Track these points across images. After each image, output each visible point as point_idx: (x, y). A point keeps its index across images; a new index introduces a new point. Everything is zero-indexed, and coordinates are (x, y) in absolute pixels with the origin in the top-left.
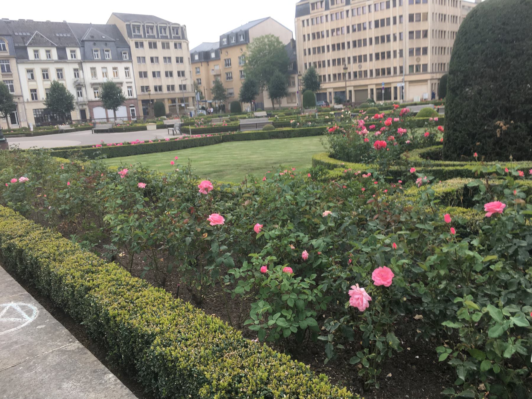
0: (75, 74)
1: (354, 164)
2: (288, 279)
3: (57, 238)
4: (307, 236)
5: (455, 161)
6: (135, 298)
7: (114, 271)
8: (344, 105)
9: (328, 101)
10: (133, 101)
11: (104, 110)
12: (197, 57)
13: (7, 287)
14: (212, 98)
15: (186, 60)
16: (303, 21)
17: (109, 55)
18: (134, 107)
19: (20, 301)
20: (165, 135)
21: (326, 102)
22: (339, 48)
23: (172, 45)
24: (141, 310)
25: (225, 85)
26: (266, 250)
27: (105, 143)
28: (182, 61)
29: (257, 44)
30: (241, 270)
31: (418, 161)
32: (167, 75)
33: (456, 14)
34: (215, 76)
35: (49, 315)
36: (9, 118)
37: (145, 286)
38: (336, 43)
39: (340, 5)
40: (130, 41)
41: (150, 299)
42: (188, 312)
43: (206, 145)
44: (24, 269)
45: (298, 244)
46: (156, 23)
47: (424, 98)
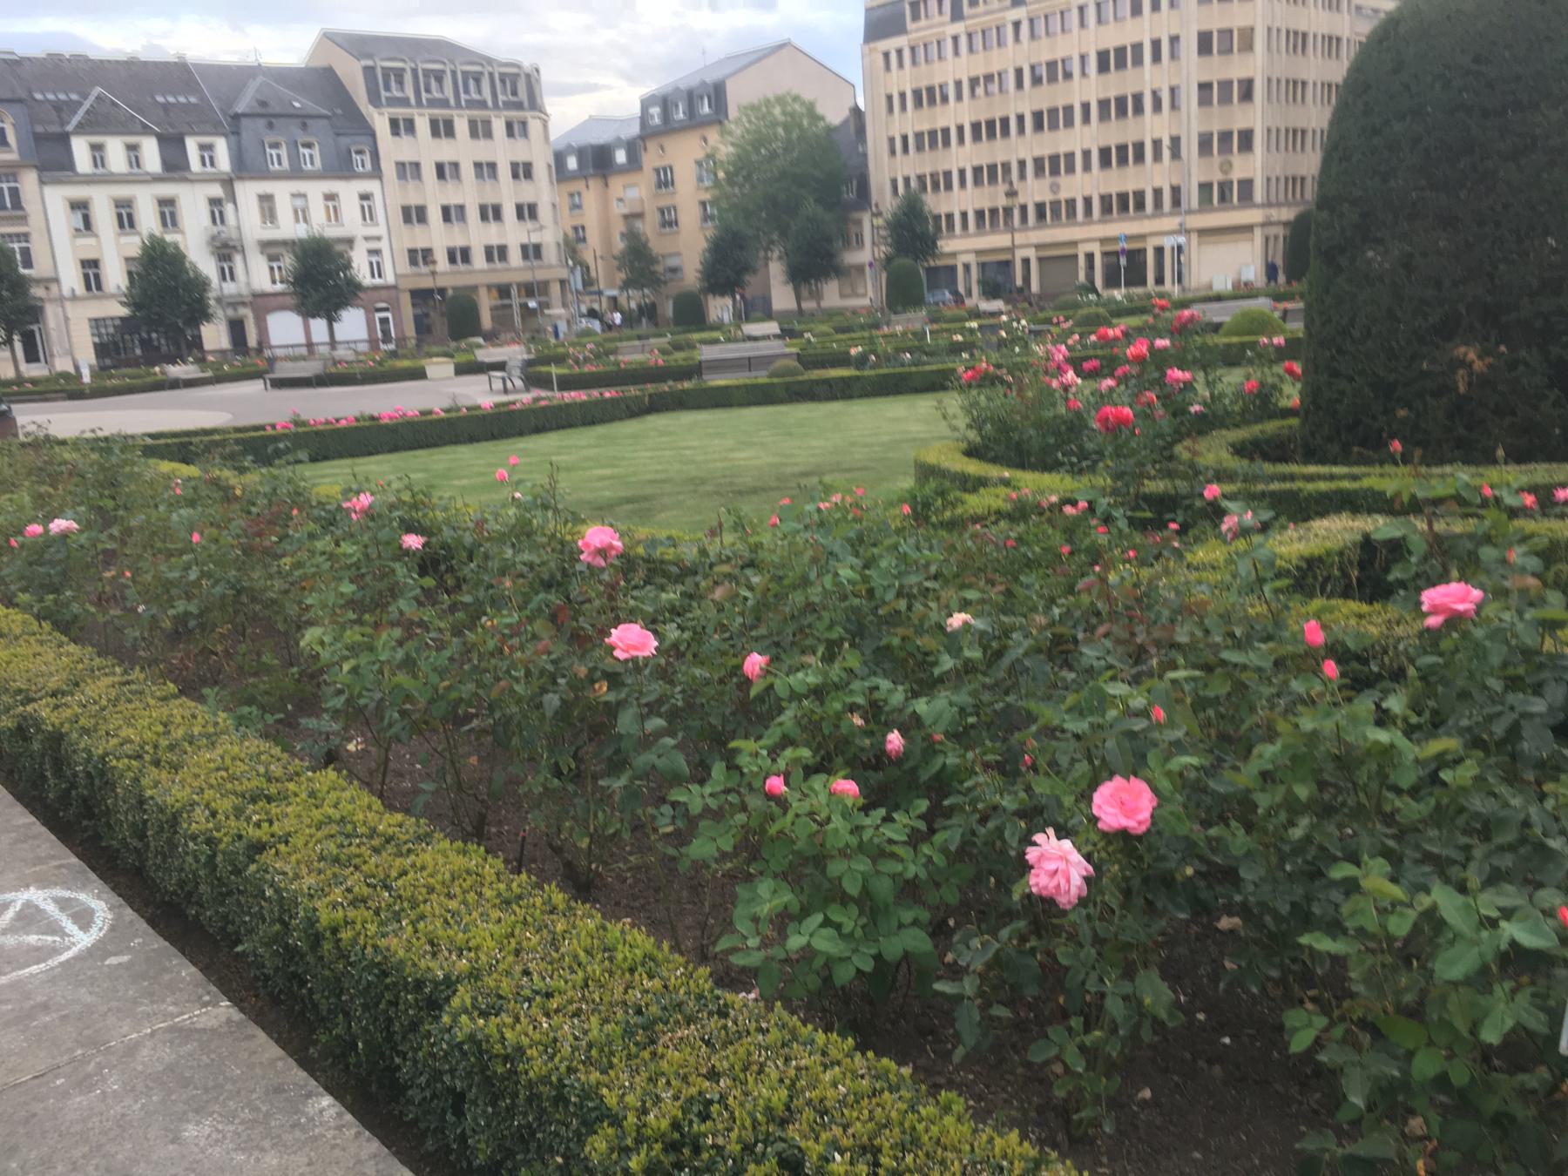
0: (213, 213)
2: (846, 815)
3: (164, 699)
4: (900, 688)
5: (1335, 463)
6: (394, 874)
7: (333, 795)
8: (1007, 302)
9: (961, 289)
10: (384, 293)
12: (572, 163)
14: (619, 283)
15: (541, 171)
16: (886, 55)
17: (313, 158)
18: (386, 310)
20: (480, 393)
21: (955, 293)
23: (498, 126)
25: (657, 245)
27: (304, 417)
29: (750, 122)
30: (708, 790)
32: (484, 217)
33: (1337, 32)
34: (626, 217)
36: (18, 346)
38: (983, 118)
40: (376, 116)
41: (439, 877)
42: (551, 912)
43: (602, 421)
45: (876, 713)
47: (1244, 278)
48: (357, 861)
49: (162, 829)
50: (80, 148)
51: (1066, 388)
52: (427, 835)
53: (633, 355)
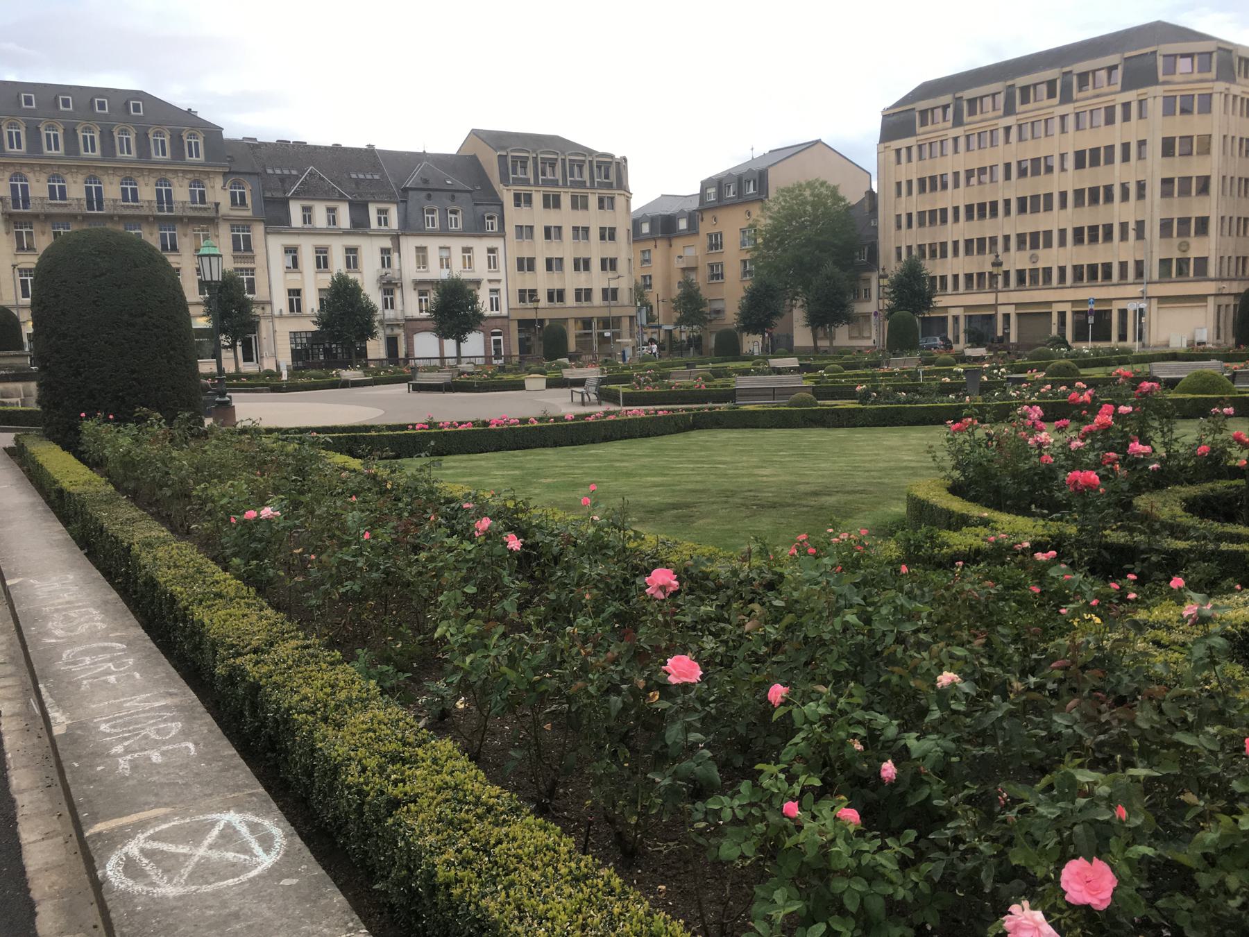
0: (383, 259)
2: (847, 838)
4: (895, 722)
6: (493, 842)
7: (450, 764)
8: (989, 350)
9: (950, 337)
10: (499, 322)
11: (437, 339)
12: (646, 228)
15: (622, 235)
16: (898, 151)
18: (499, 334)
20: (564, 405)
21: (945, 339)
22: (982, 215)
24: (506, 875)
25: (705, 292)
26: (794, 749)
27: (436, 420)
28: (612, 237)
29: (785, 201)
30: (736, 803)
31: (1179, 519)
32: (577, 268)
34: (684, 269)
35: (307, 853)
37: (515, 811)
38: (975, 201)
39: (991, 114)
41: (526, 850)
42: (610, 894)
43: (656, 434)
44: (258, 729)
45: (872, 738)
46: (563, 153)
47: (1197, 339)
50: (295, 210)
51: (1040, 446)
52: (518, 808)
53: (682, 379)
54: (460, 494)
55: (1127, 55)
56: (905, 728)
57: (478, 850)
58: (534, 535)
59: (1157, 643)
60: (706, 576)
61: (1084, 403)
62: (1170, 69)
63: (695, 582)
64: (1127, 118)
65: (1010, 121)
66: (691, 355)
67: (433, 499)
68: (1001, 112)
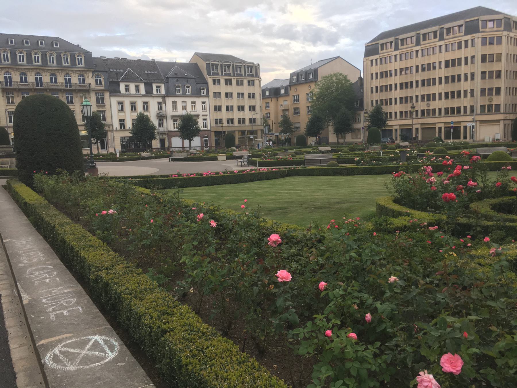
0: (158, 106)
1: (419, 212)
2: (352, 346)
3: (138, 274)
4: (371, 297)
6: (205, 347)
8: (410, 143)
9: (394, 138)
10: (207, 132)
12: (267, 93)
13: (93, 318)
14: (279, 131)
16: (372, 61)
18: (207, 137)
19: (104, 334)
20: (234, 166)
21: (391, 138)
22: (407, 87)
23: (245, 82)
24: (211, 361)
25: (292, 120)
26: (329, 308)
27: (181, 173)
29: (325, 82)
30: (306, 331)
31: (488, 213)
32: (239, 110)
34: (283, 110)
36: (99, 144)
37: (214, 334)
38: (404, 81)
42: (254, 369)
43: (272, 179)
46: (233, 62)
47: (496, 138)
48: (194, 341)
49: (136, 319)
50: (122, 86)
51: (431, 183)
52: (215, 333)
53: (282, 156)
54: (191, 204)
55: (467, 20)
56: (375, 299)
57: (199, 351)
58: (222, 221)
59: (480, 264)
60: (293, 237)
61: (450, 165)
62: (485, 26)
63: (288, 239)
64: (466, 46)
65: (418, 48)
66: (287, 146)
67: (180, 206)
68: (414, 44)
